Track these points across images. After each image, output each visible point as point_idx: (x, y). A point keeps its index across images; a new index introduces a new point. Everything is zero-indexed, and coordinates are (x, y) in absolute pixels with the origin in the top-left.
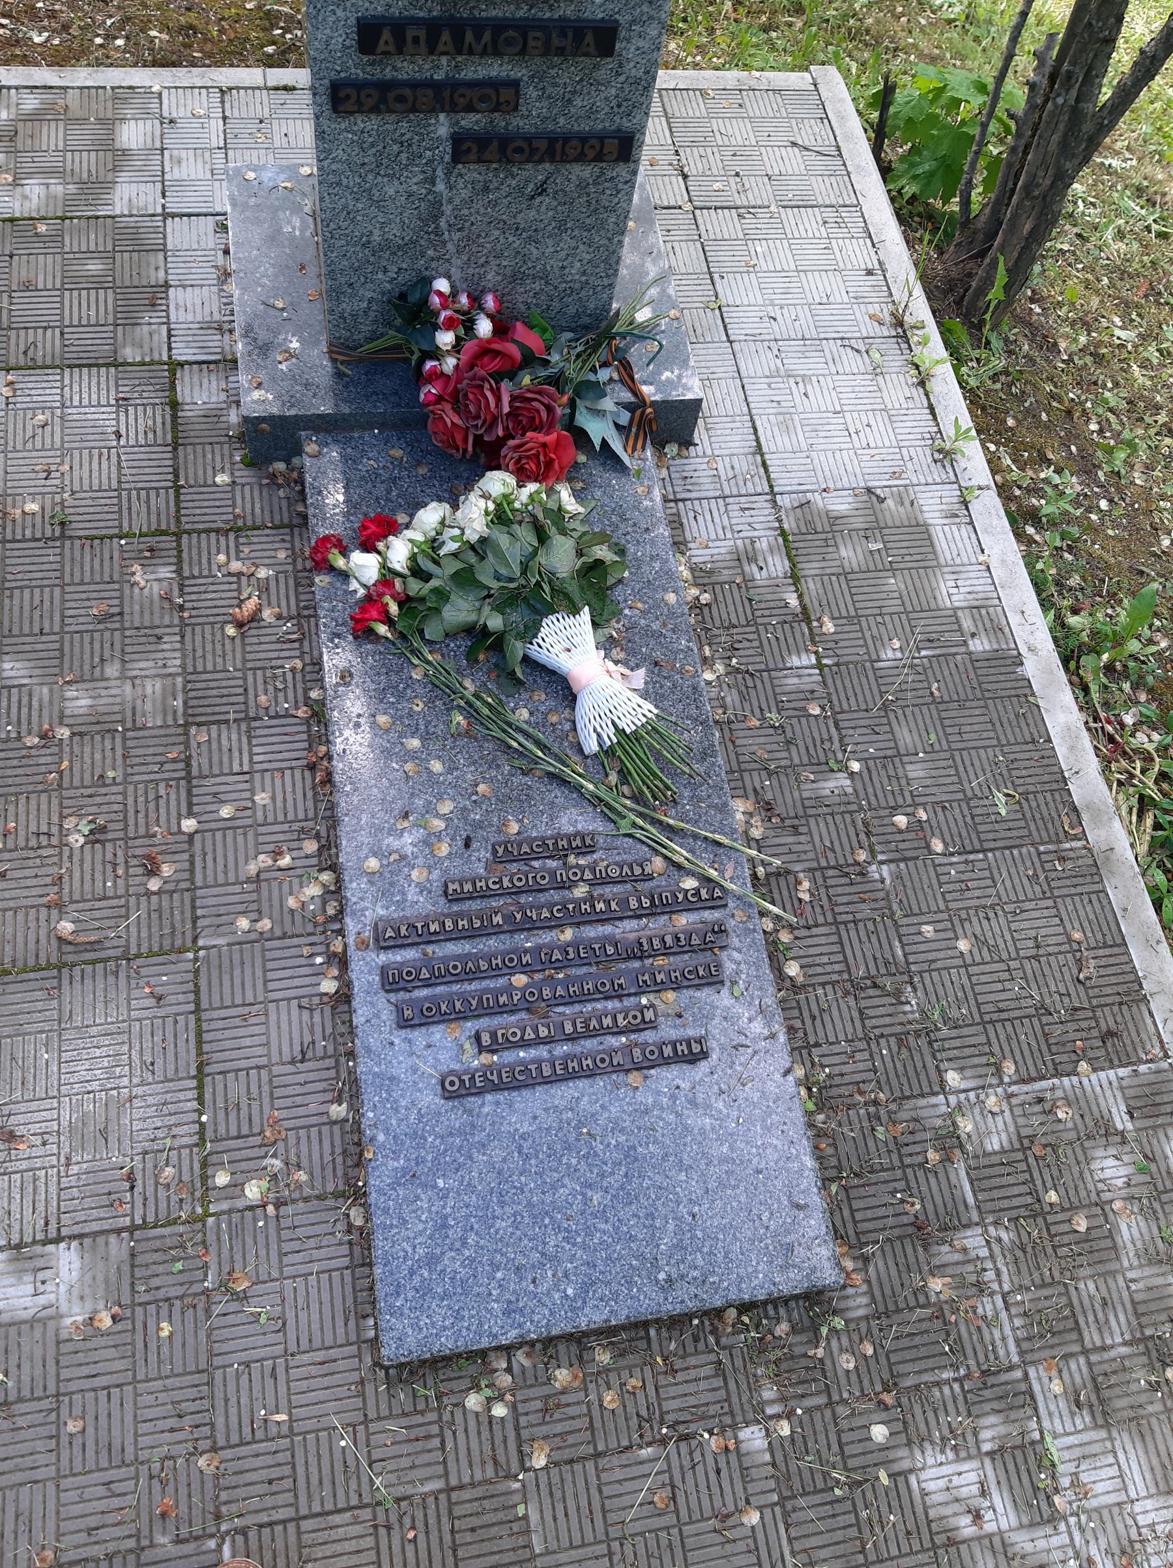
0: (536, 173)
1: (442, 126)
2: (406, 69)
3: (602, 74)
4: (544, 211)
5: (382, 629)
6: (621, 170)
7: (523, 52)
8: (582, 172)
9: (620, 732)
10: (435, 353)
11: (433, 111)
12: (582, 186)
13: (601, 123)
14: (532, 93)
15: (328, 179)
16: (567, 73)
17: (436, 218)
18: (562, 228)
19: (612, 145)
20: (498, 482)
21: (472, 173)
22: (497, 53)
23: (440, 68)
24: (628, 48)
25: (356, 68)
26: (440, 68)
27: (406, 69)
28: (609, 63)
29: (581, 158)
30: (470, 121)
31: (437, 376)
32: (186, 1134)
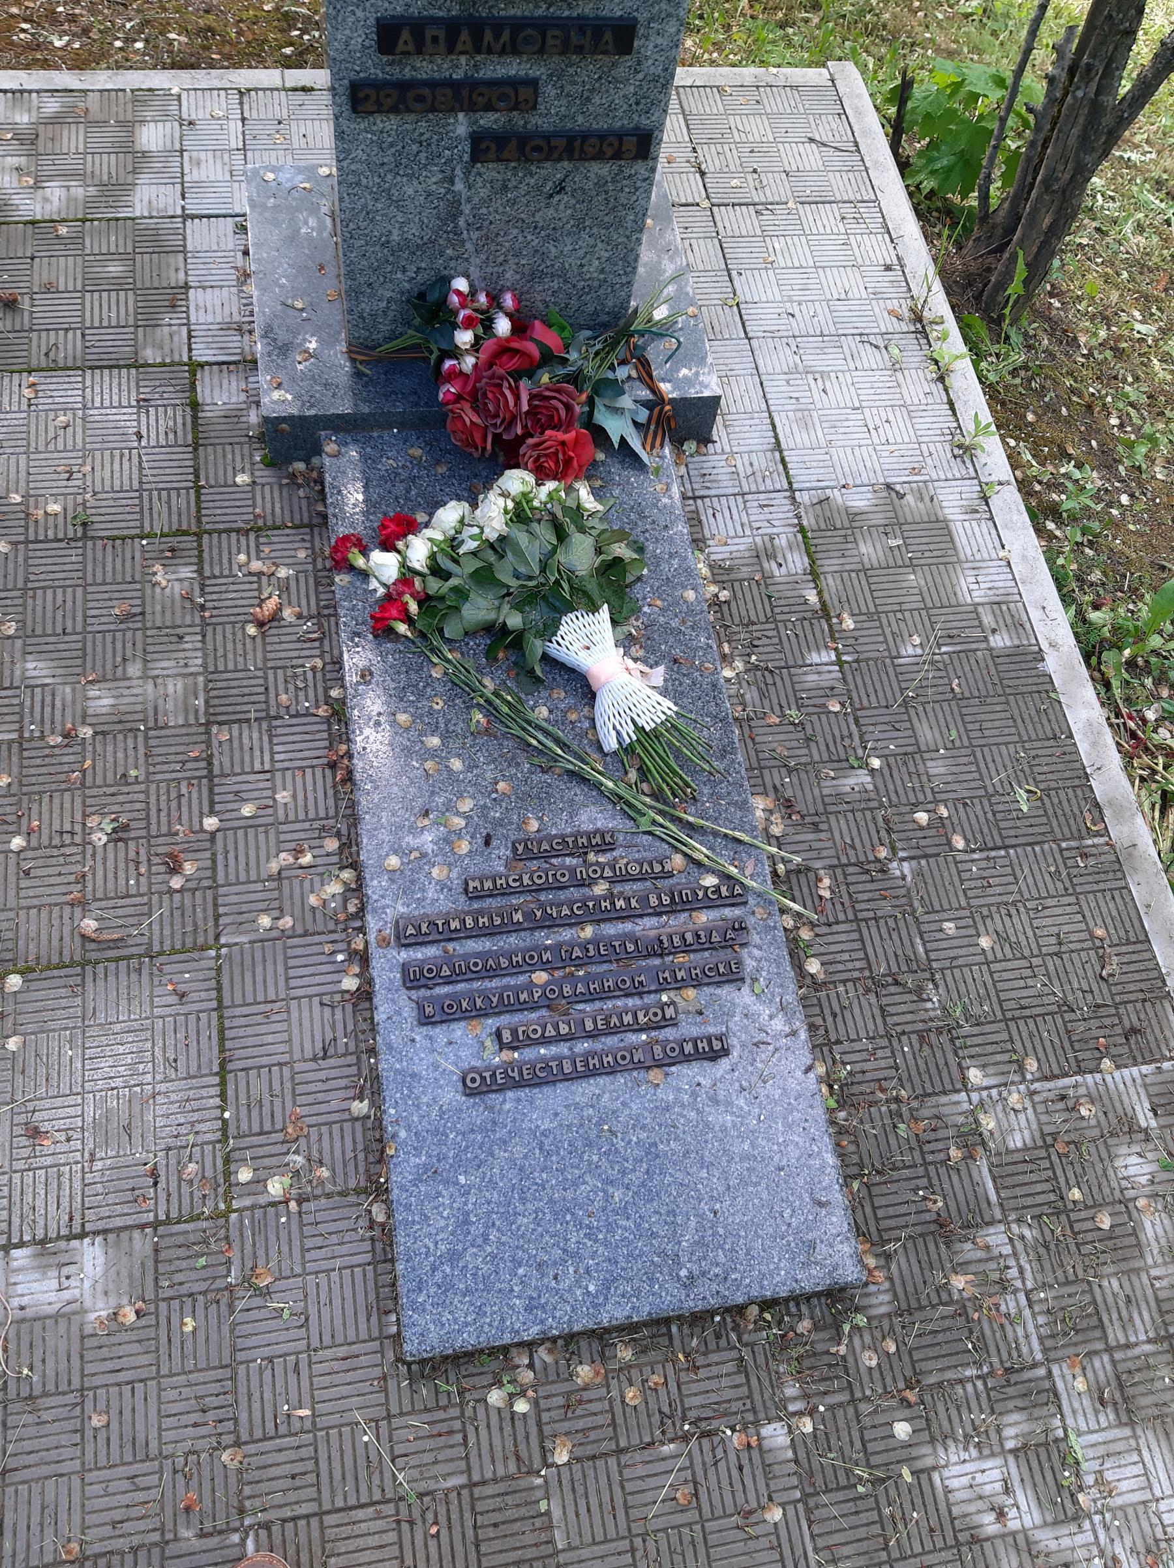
0: (552, 172)
1: (461, 125)
2: (425, 68)
3: (621, 72)
4: (562, 209)
5: (402, 628)
6: (640, 167)
7: (541, 51)
8: (600, 170)
9: (639, 729)
10: (454, 352)
11: (452, 110)
12: (601, 184)
13: (620, 121)
14: (550, 91)
15: (348, 180)
16: (586, 71)
17: (454, 217)
18: (580, 226)
19: (630, 143)
20: (517, 481)
21: (491, 171)
22: (516, 52)
23: (459, 67)
24: (647, 46)
25: (375, 68)
26: (459, 67)
27: (425, 68)
28: (628, 61)
29: (599, 156)
30: (489, 120)
31: (455, 375)
32: (209, 1130)
